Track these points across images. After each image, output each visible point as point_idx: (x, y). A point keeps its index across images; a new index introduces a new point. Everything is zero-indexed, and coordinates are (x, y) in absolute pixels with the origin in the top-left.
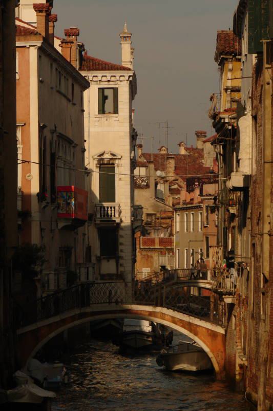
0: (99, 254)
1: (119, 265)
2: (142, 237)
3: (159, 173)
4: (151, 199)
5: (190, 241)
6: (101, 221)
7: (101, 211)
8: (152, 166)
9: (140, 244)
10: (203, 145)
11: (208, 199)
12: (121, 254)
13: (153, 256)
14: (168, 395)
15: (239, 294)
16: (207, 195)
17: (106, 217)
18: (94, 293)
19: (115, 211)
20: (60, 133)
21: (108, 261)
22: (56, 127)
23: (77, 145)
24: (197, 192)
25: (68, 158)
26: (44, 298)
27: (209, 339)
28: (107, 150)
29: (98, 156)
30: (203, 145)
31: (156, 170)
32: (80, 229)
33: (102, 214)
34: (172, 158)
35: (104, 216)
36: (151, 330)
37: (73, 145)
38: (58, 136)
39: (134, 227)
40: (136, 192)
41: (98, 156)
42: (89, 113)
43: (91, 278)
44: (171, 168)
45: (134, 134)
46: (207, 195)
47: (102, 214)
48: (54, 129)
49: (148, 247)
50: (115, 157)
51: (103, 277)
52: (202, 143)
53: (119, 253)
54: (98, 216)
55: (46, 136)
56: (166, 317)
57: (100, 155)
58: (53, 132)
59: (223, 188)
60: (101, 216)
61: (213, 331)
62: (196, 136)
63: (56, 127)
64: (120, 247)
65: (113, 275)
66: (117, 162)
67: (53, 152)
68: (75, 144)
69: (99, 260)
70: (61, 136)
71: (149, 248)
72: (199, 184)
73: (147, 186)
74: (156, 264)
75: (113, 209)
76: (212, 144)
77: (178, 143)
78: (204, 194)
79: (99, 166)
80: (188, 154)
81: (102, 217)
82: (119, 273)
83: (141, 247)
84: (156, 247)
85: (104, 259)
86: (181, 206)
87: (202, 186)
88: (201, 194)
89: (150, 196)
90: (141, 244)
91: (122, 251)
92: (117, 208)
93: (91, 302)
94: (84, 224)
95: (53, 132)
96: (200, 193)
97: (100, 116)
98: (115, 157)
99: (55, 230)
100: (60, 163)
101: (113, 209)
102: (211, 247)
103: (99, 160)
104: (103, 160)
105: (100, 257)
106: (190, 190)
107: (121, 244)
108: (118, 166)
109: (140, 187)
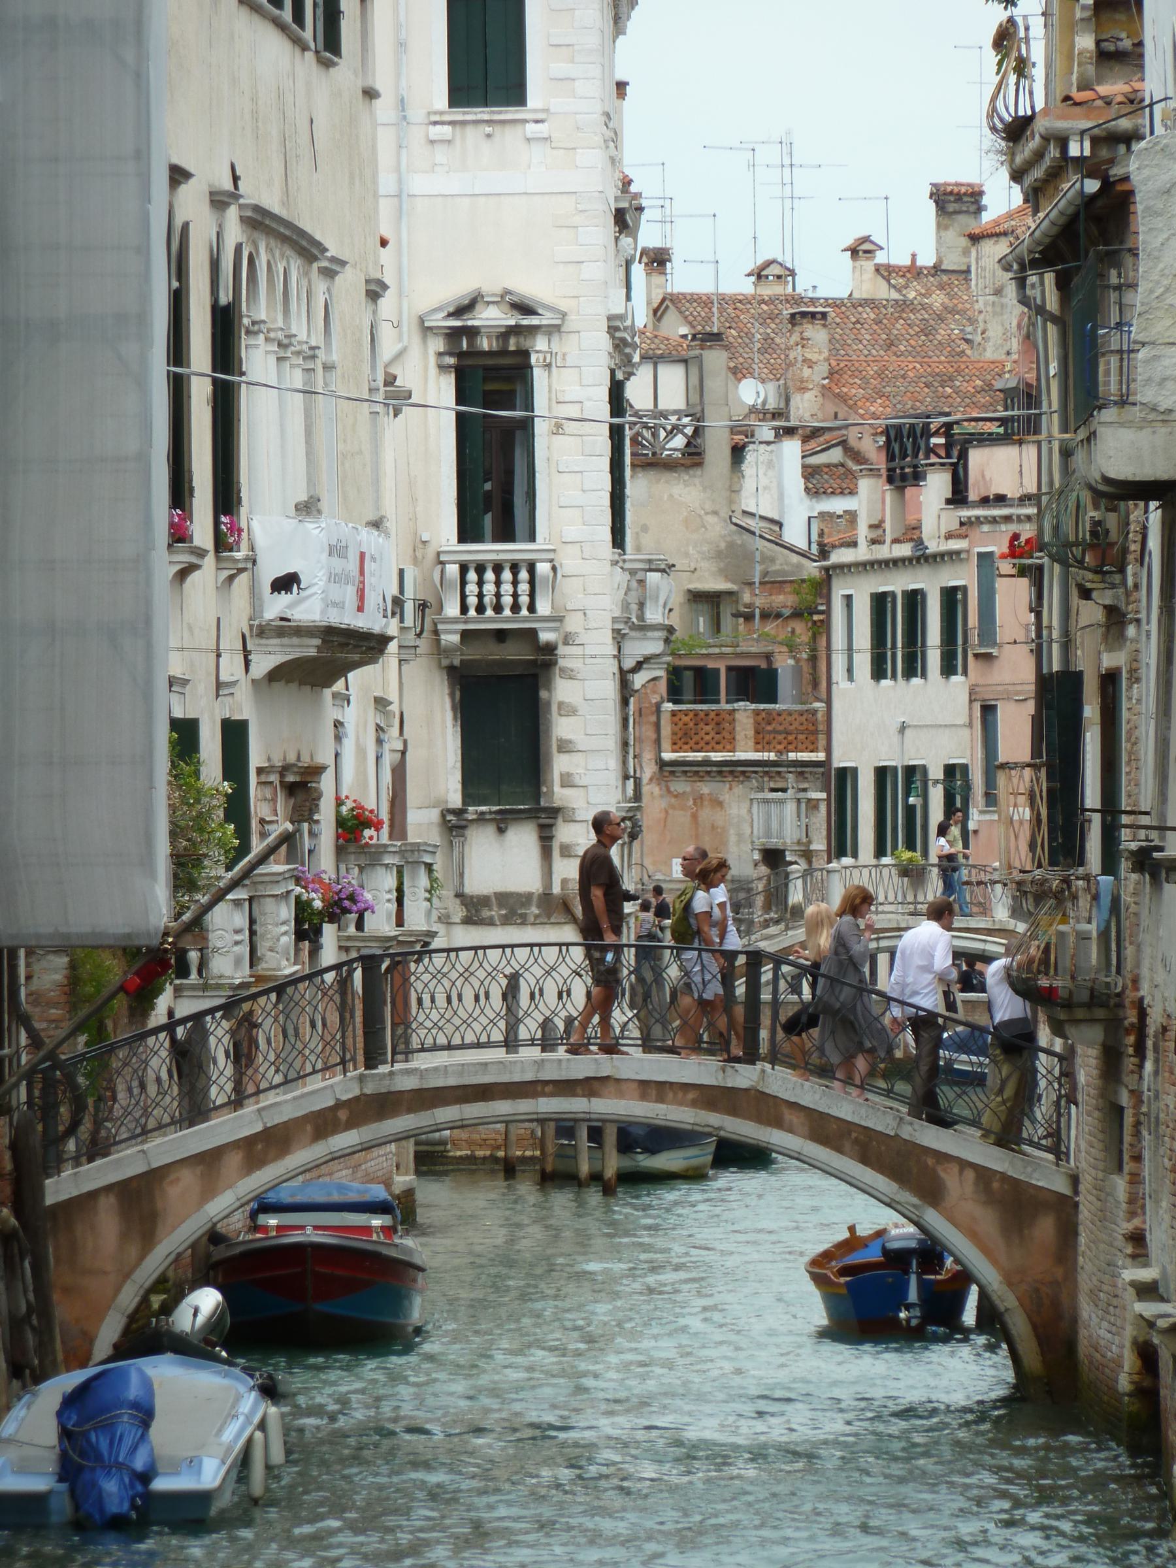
0: (455, 799)
1: (556, 853)
2: (669, 706)
3: (750, 392)
4: (711, 519)
5: (903, 728)
6: (465, 634)
7: (463, 583)
8: (715, 359)
9: (658, 741)
10: (966, 252)
11: (994, 521)
12: (560, 795)
13: (726, 797)
14: (793, 1494)
15: (1142, 999)
16: (985, 501)
17: (489, 612)
18: (426, 998)
19: (532, 582)
20: (257, 208)
21: (501, 831)
22: (236, 179)
23: (343, 263)
24: (937, 484)
25: (299, 328)
26: (183, 1021)
27: (987, 1220)
28: (491, 286)
29: (450, 315)
30: (966, 252)
31: (738, 373)
32: (361, 681)
33: (472, 601)
34: (813, 315)
35: (480, 609)
36: (825, 1322)
37: (325, 264)
38: (246, 221)
39: (629, 664)
40: (636, 487)
41: (450, 315)
42: (402, 103)
43: (417, 918)
44: (810, 363)
45: (624, 205)
46: (985, 501)
47: (472, 601)
48: (228, 185)
49: (699, 756)
50: (533, 321)
51: (476, 910)
52: (964, 242)
53: (557, 788)
54: (452, 609)
55: (186, 226)
56: (789, 1116)
57: (461, 311)
58: (219, 201)
59: (1057, 485)
60: (464, 609)
61: (1015, 1182)
62: (932, 205)
63: (236, 179)
64: (560, 764)
65: (525, 899)
66: (540, 343)
67: (224, 300)
68: (333, 260)
69: (454, 825)
70: (260, 221)
71: (706, 763)
72: (948, 447)
73: (693, 456)
74: (740, 836)
75: (524, 575)
76: (723, 865)
77: (849, 242)
78: (973, 496)
79: (452, 361)
80: (895, 295)
81: (472, 613)
82: (556, 889)
83: (667, 756)
84: (741, 756)
85: (481, 819)
86: (862, 553)
87: (963, 456)
88: (958, 496)
89: (708, 506)
90: (666, 743)
91: (567, 781)
92: (542, 568)
93: (415, 1043)
94: (381, 651)
95: (219, 201)
96: (954, 492)
97: (459, 114)
98: (533, 321)
99: (234, 684)
100: (257, 359)
101: (524, 575)
102: (1003, 766)
103: (454, 335)
104: (472, 333)
105: (459, 813)
106: (903, 477)
107: (565, 747)
108: (548, 366)
109: (653, 463)
